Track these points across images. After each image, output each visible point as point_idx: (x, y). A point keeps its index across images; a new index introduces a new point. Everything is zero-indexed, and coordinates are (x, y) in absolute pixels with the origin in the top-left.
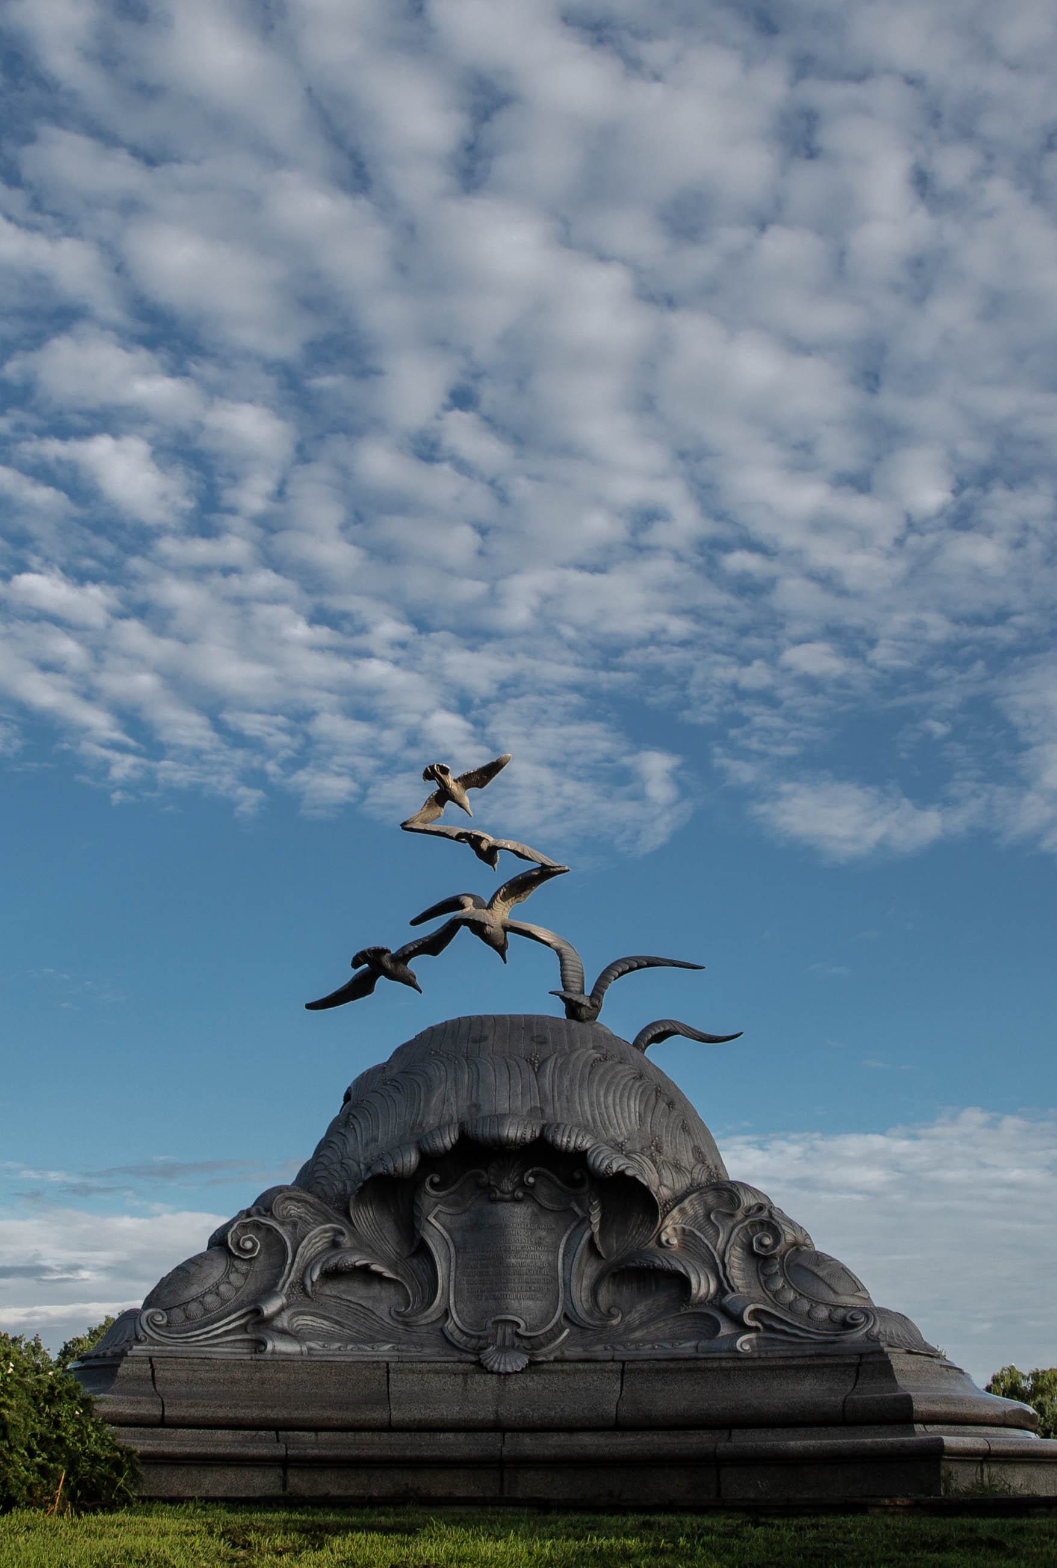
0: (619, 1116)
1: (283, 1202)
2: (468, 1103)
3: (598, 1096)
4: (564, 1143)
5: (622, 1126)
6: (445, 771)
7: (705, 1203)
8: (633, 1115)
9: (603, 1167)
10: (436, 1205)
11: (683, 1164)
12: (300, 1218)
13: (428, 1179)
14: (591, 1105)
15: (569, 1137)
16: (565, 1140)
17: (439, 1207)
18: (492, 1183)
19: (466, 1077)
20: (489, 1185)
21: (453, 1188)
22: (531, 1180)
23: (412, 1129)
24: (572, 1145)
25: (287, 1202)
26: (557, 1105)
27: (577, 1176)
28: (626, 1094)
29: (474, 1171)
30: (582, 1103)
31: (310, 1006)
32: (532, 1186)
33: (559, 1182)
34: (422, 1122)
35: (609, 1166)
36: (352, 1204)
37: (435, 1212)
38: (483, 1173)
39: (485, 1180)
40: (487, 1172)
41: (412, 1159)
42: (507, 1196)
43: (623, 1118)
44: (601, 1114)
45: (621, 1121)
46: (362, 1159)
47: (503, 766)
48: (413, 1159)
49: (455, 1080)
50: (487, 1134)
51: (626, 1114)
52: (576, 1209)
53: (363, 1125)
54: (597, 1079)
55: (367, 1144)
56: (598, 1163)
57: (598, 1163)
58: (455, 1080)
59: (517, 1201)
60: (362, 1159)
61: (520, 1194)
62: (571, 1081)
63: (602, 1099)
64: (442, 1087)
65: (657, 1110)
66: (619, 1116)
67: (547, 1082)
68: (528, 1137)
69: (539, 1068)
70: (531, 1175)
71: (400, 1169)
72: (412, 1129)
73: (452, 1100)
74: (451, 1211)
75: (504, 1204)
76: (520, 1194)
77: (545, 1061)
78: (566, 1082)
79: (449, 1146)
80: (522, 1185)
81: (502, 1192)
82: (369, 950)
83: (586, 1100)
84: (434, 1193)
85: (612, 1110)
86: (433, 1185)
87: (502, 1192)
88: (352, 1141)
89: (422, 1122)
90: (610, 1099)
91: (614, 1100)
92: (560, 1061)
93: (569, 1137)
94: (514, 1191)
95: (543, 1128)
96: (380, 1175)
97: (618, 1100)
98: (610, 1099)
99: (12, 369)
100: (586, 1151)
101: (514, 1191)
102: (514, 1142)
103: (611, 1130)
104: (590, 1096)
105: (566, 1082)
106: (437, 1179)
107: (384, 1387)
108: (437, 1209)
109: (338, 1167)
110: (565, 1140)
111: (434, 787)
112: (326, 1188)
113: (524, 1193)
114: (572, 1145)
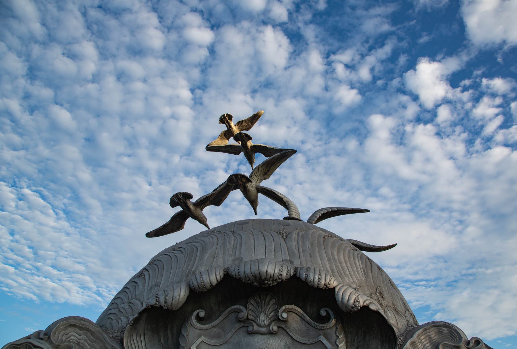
0: (350, 269)
1: (66, 329)
2: (233, 258)
3: (333, 255)
4: (317, 280)
5: (354, 276)
6: (230, 117)
7: (430, 338)
8: (359, 269)
9: (352, 301)
10: (199, 336)
11: (399, 309)
12: (78, 344)
13: (195, 314)
14: (329, 260)
15: (320, 275)
16: (317, 277)
17: (202, 338)
18: (251, 317)
19: (232, 242)
20: (248, 319)
21: (216, 322)
22: (285, 315)
23: (187, 276)
24: (323, 282)
25: (70, 329)
26: (303, 258)
27: (323, 313)
28: (352, 256)
29: (235, 307)
30: (322, 259)
31: (149, 235)
32: (285, 321)
33: (308, 318)
34: (195, 270)
35: (356, 300)
36: (126, 333)
37: (198, 342)
38: (243, 308)
39: (244, 314)
40: (246, 308)
41: (181, 294)
42: (264, 330)
43: (353, 271)
44: (337, 267)
45: (352, 273)
46: (145, 300)
47: (259, 117)
48: (182, 294)
49: (224, 244)
50: (248, 271)
51: (355, 269)
52: (325, 342)
53: (151, 275)
54: (330, 245)
55: (151, 288)
56: (346, 298)
57: (346, 298)
58: (224, 244)
59: (272, 333)
60: (145, 300)
61: (275, 328)
62: (312, 244)
63: (336, 257)
64: (214, 247)
65: (373, 269)
66: (350, 269)
67: (293, 244)
68: (284, 274)
69: (286, 236)
70: (284, 311)
71: (170, 301)
72: (187, 276)
73: (221, 256)
74: (212, 342)
75: (260, 337)
76: (275, 328)
77: (290, 233)
78: (308, 244)
79: (214, 282)
80: (277, 319)
81: (259, 325)
82: (180, 193)
83: (324, 255)
84: (199, 325)
85: (344, 265)
86: (199, 319)
87: (259, 325)
88: (141, 286)
89: (195, 270)
90: (342, 257)
91: (344, 258)
92: (301, 234)
93: (320, 275)
94: (269, 325)
95: (296, 270)
96: (153, 307)
97: (347, 260)
98: (342, 257)
99: (70, 6)
100: (334, 288)
101: (269, 325)
102: (272, 278)
103: (346, 279)
104: (327, 254)
105: (308, 244)
106: (202, 314)
107: (288, 245)
108: (200, 340)
109: (126, 306)
110: (317, 277)
111: (224, 128)
112: (114, 322)
113: (278, 327)
114: (323, 282)
